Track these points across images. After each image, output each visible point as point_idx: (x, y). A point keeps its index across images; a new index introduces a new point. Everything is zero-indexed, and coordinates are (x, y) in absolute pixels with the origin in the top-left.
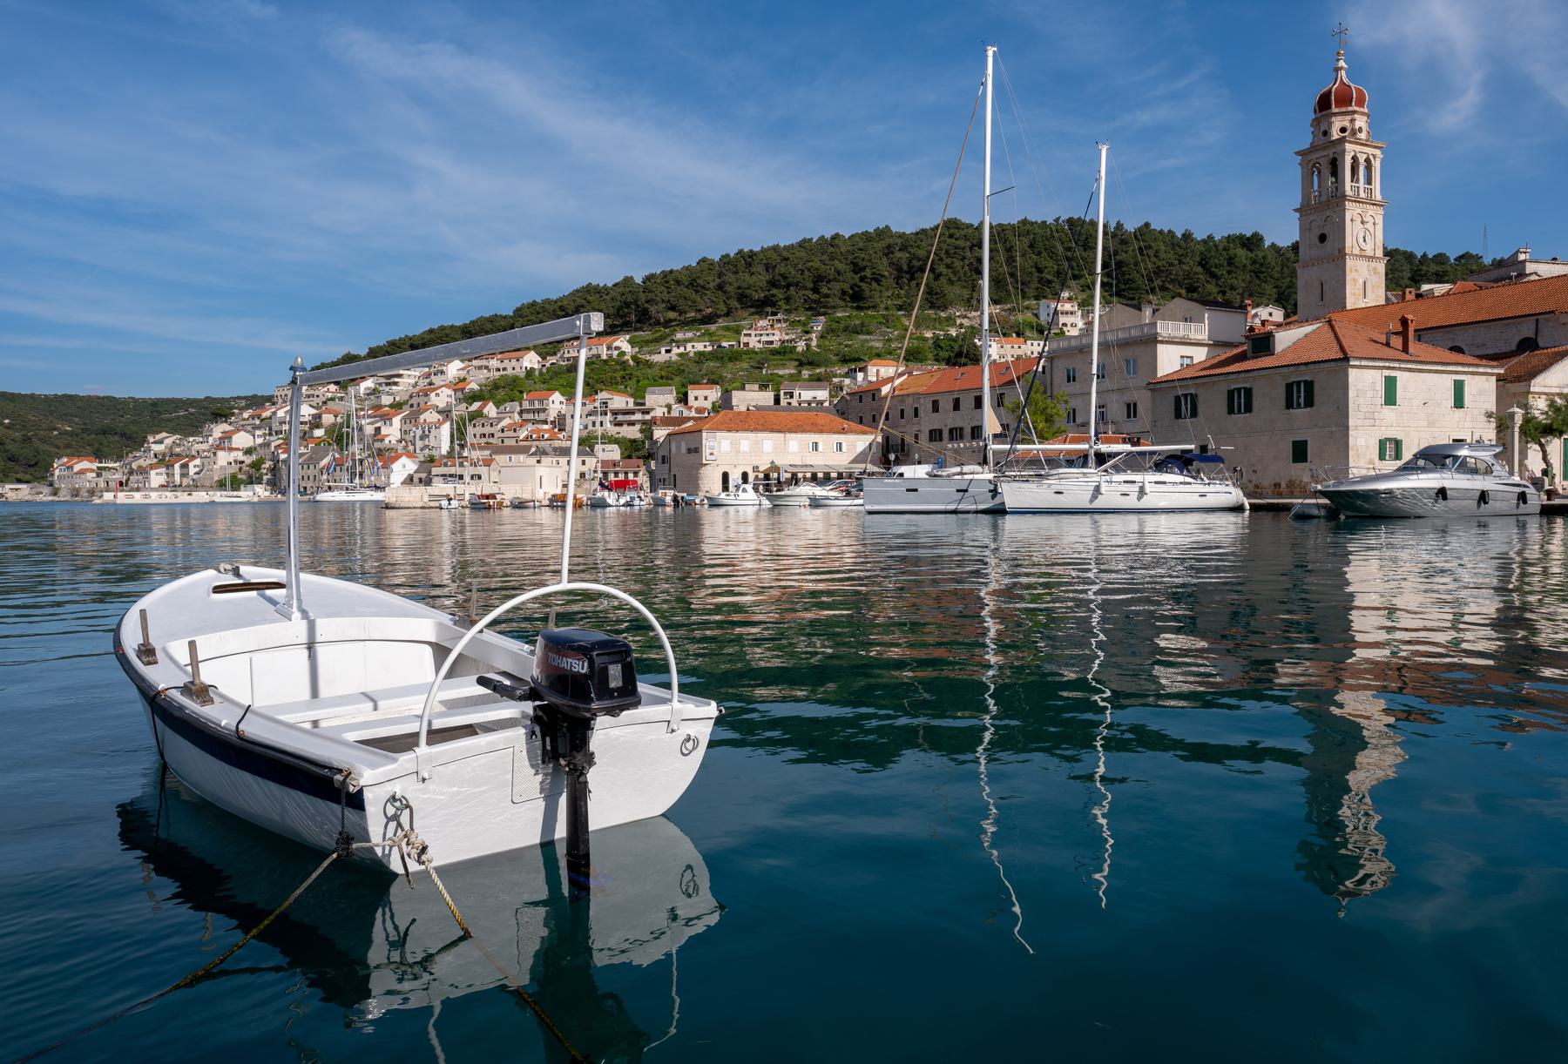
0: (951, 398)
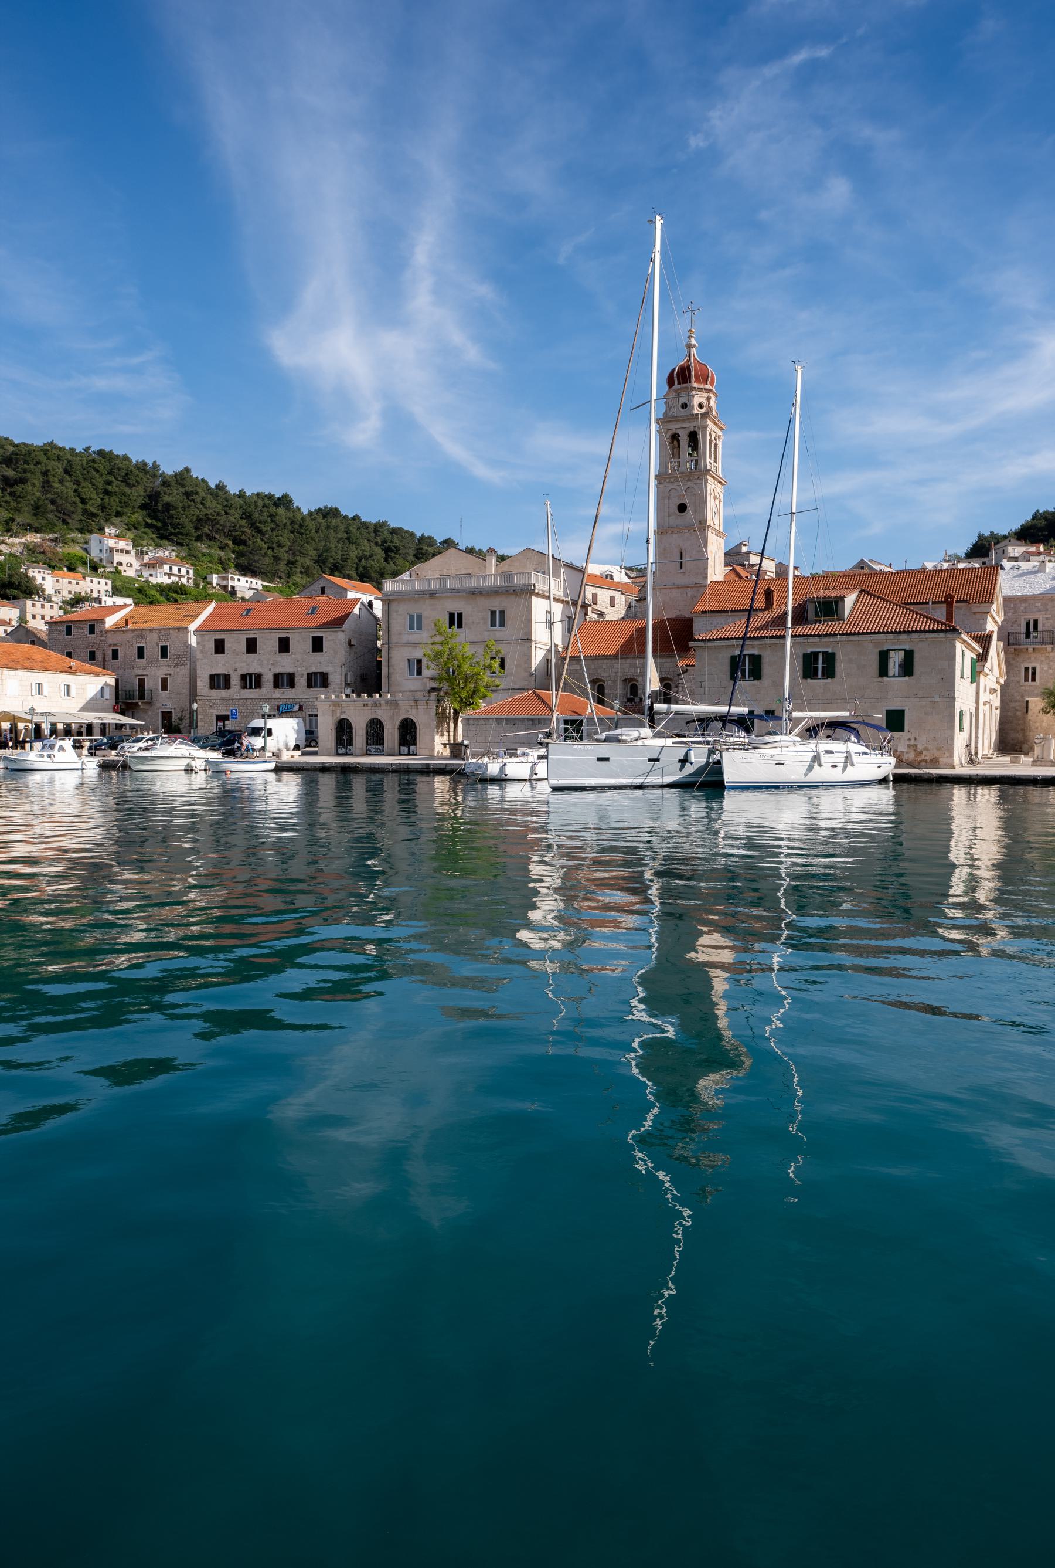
0: (276, 636)
